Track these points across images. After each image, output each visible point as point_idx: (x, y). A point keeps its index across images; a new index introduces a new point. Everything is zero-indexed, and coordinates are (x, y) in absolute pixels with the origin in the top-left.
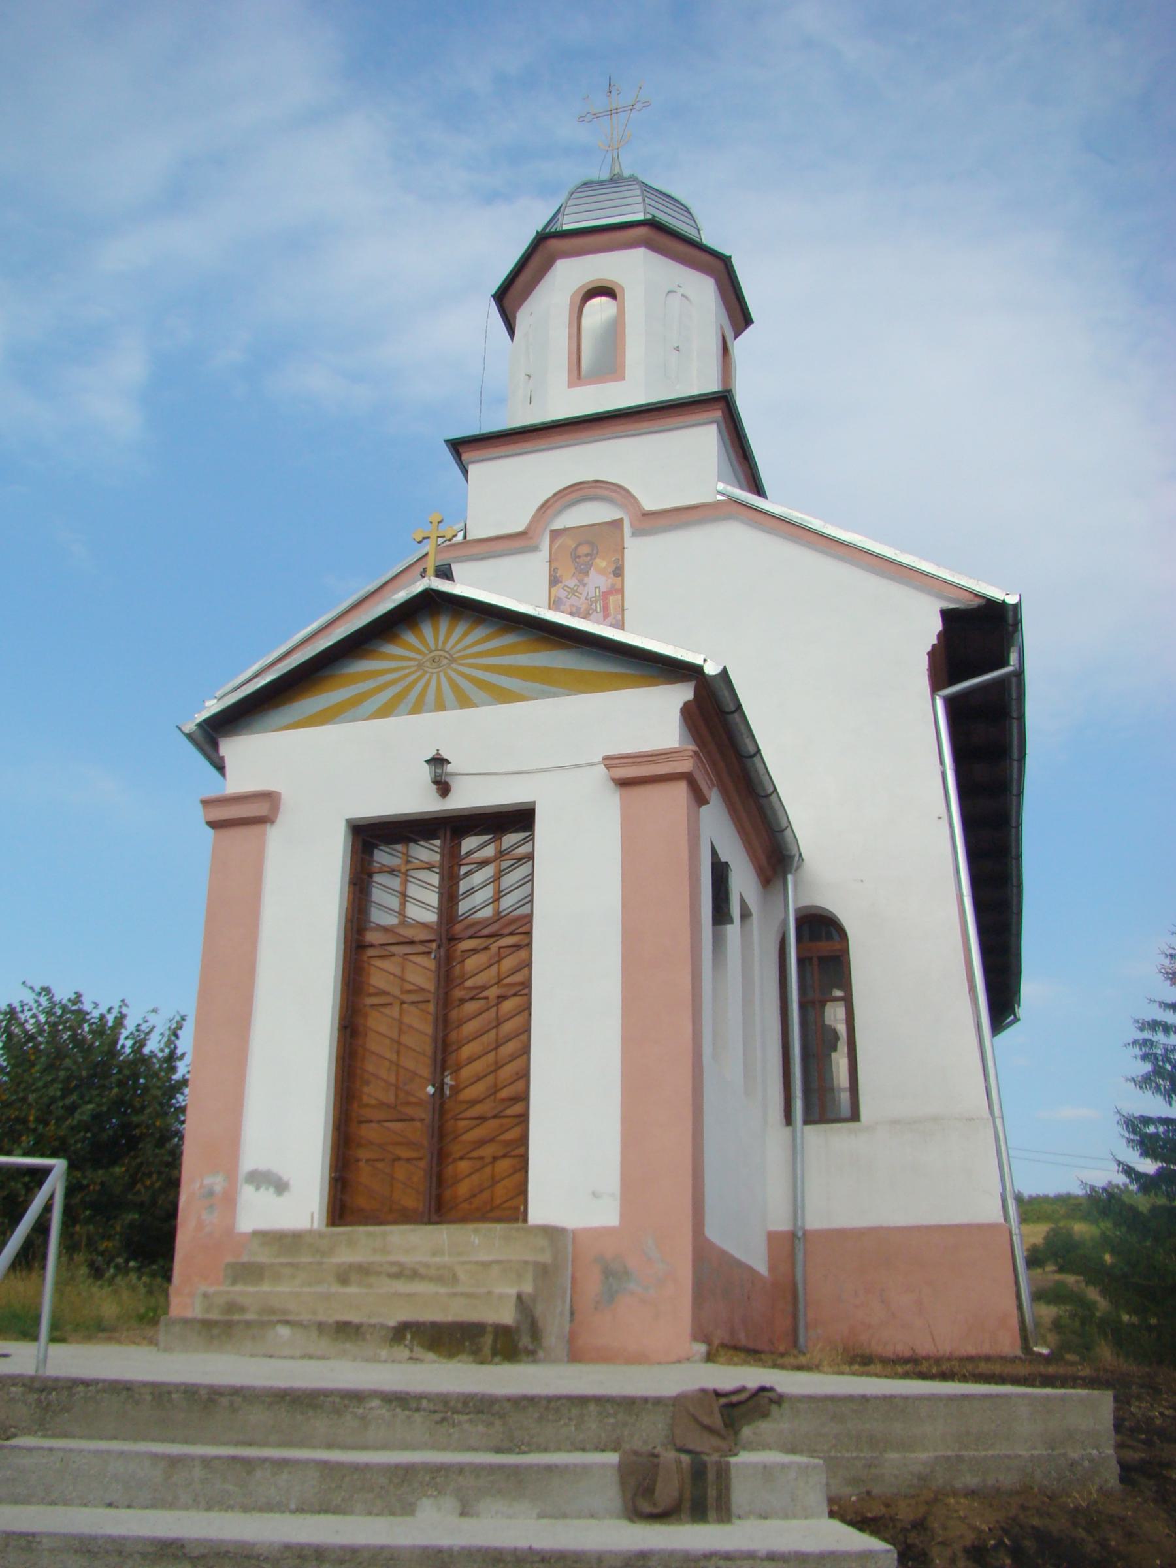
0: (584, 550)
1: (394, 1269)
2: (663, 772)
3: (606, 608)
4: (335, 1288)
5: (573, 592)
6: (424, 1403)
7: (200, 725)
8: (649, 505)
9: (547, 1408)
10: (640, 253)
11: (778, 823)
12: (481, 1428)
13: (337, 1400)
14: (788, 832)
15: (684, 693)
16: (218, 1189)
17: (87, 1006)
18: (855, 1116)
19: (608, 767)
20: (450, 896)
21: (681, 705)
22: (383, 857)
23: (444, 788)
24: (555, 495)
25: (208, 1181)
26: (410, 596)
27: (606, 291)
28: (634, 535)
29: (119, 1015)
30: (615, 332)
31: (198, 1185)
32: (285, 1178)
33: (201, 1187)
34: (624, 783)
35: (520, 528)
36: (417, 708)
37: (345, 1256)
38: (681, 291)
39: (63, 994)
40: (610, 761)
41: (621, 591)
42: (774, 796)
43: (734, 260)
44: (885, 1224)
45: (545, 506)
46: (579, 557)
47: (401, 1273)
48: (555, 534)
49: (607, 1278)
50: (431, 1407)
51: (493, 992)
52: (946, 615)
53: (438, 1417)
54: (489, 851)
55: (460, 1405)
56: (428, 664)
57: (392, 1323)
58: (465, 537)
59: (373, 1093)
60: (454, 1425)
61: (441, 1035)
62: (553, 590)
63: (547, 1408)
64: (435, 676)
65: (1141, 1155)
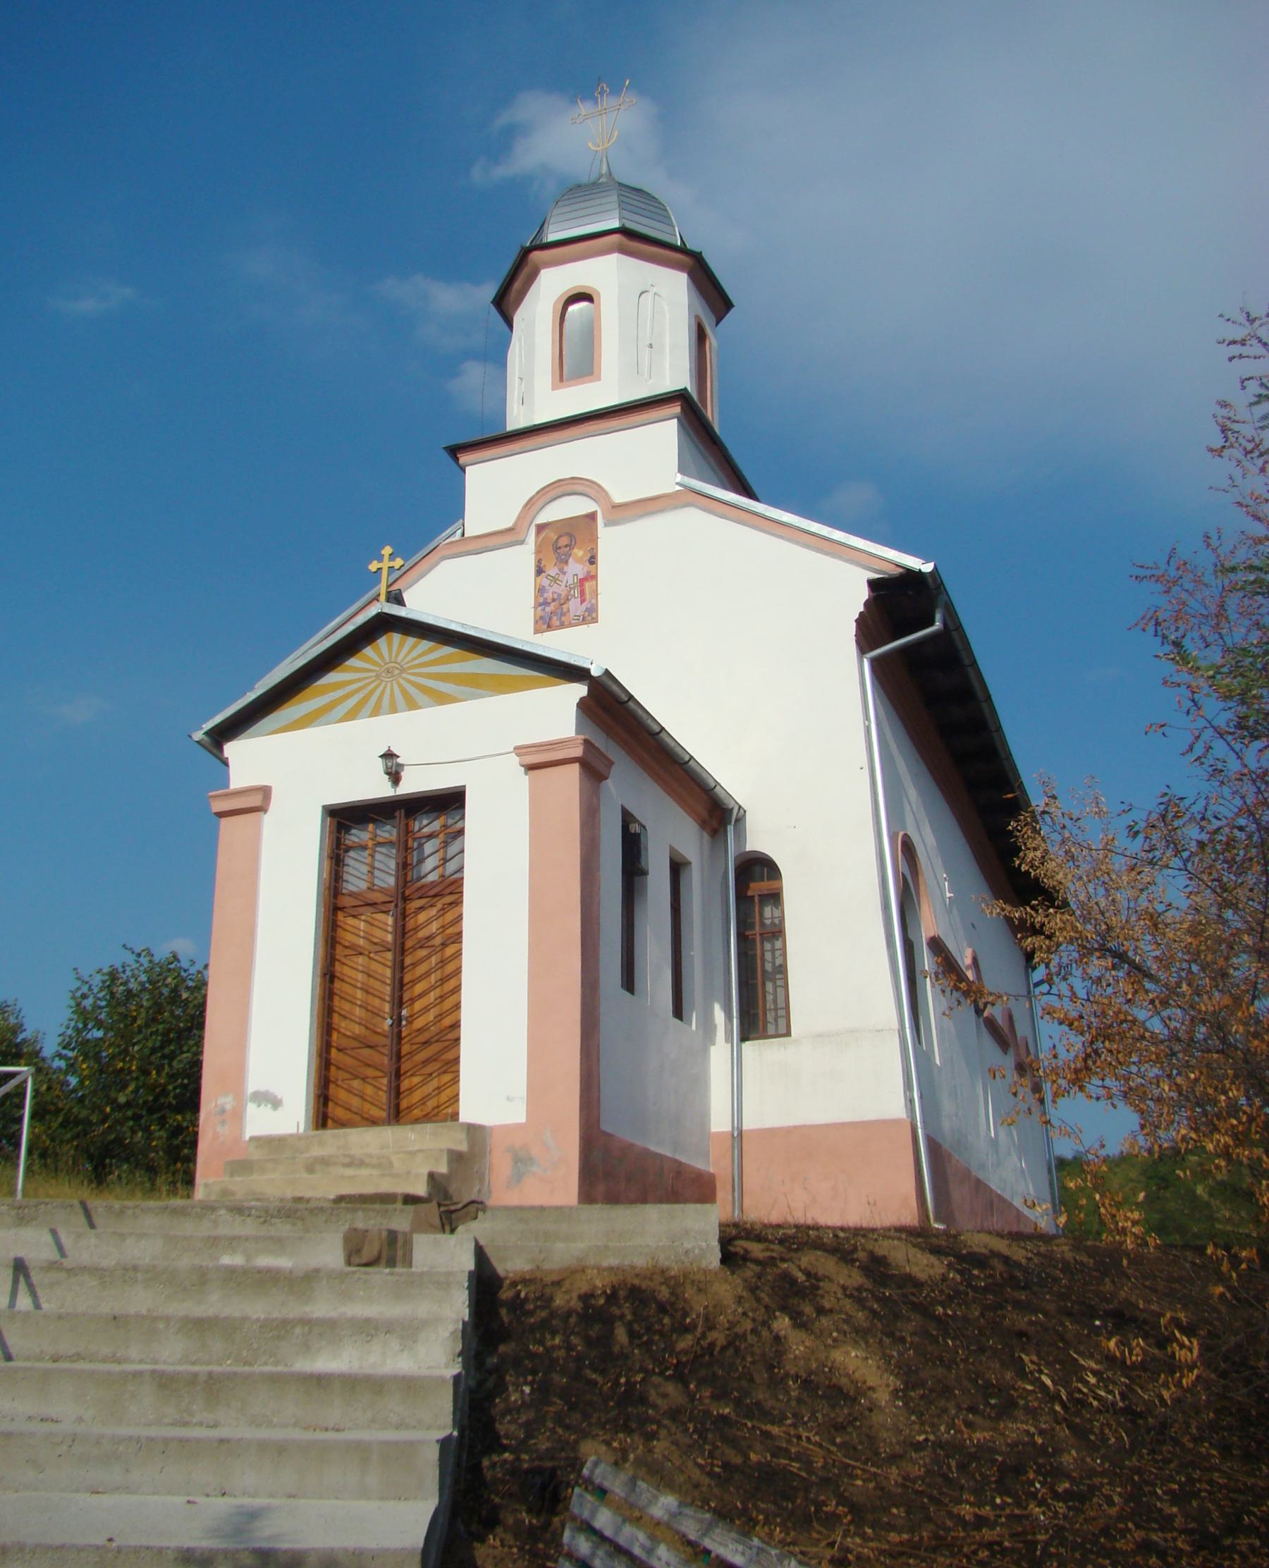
0: (564, 541)
1: (347, 1160)
2: (560, 758)
3: (582, 593)
4: (305, 1175)
5: (555, 580)
6: (253, 1212)
7: (207, 733)
8: (618, 498)
9: (331, 1214)
10: (615, 257)
11: (708, 785)
12: (288, 1227)
13: (199, 1210)
14: (718, 789)
15: (580, 690)
16: (228, 1107)
17: (185, 963)
18: (788, 1034)
19: (518, 755)
20: (404, 866)
21: (577, 700)
22: (359, 835)
23: (395, 777)
24: (538, 492)
25: (221, 1101)
26: (367, 619)
27: (583, 296)
28: (606, 525)
29: (1038, 926)
30: (590, 335)
31: (213, 1104)
32: (279, 1097)
33: (216, 1106)
34: (530, 768)
35: (509, 524)
36: (376, 712)
37: (316, 1152)
38: (655, 289)
39: (162, 954)
40: (520, 750)
41: (594, 577)
42: (691, 763)
43: (704, 255)
44: (808, 1123)
45: (530, 503)
46: (560, 548)
47: (354, 1162)
48: (540, 528)
49: (516, 1163)
50: (257, 1213)
51: (438, 941)
52: (872, 584)
53: (261, 1220)
54: (436, 826)
55: (275, 1213)
56: (384, 674)
57: (332, 1197)
58: (463, 535)
59: (347, 1027)
60: (271, 1225)
61: (397, 977)
62: (539, 579)
63: (331, 1214)
64: (389, 684)
65: (714, 1044)
